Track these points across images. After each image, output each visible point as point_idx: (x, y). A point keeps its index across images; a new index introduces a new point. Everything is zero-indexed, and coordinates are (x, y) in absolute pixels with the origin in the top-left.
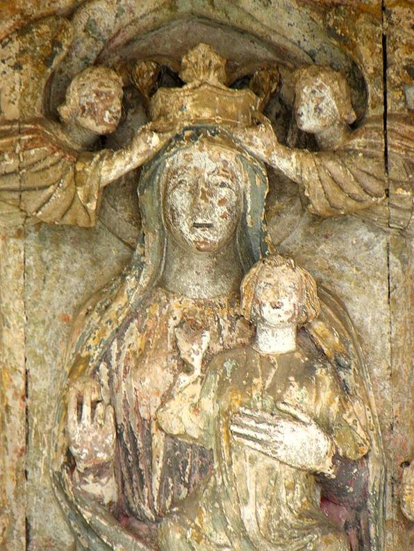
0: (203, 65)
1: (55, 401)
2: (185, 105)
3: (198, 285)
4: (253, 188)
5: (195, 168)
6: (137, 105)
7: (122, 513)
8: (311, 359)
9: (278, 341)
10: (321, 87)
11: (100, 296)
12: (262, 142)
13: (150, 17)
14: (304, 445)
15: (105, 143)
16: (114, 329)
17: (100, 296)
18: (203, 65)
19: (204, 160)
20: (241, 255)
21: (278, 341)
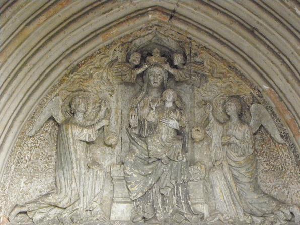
12: (167, 67)
19: (156, 70)
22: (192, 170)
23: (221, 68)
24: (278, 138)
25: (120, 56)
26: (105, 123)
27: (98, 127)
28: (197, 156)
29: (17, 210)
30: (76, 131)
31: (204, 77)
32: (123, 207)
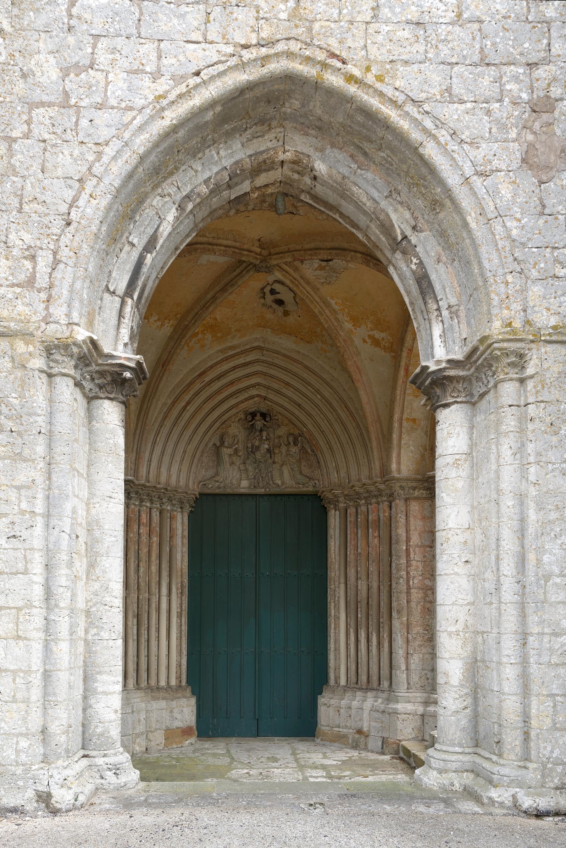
0: (258, 414)
1: (526, 144)
2: (257, 418)
3: (258, 433)
4: (262, 425)
5: (7, 259)
6: (253, 419)
7: (252, 452)
8: (267, 439)
9: (264, 438)
10: (522, 9)
11: (250, 434)
12: (263, 421)
13: (140, 170)
14: (266, 446)
15: (251, 421)
16: (33, 664)
17: (250, 434)
18: (258, 414)
19: (258, 423)
20: (261, 431)
21: (264, 438)
22: (274, 466)
23: (286, 422)
24: (310, 451)
25: (243, 416)
26: (236, 446)
27: (234, 448)
28: (276, 460)
29: (202, 483)
30: (225, 450)
31: (279, 426)
32: (245, 482)
